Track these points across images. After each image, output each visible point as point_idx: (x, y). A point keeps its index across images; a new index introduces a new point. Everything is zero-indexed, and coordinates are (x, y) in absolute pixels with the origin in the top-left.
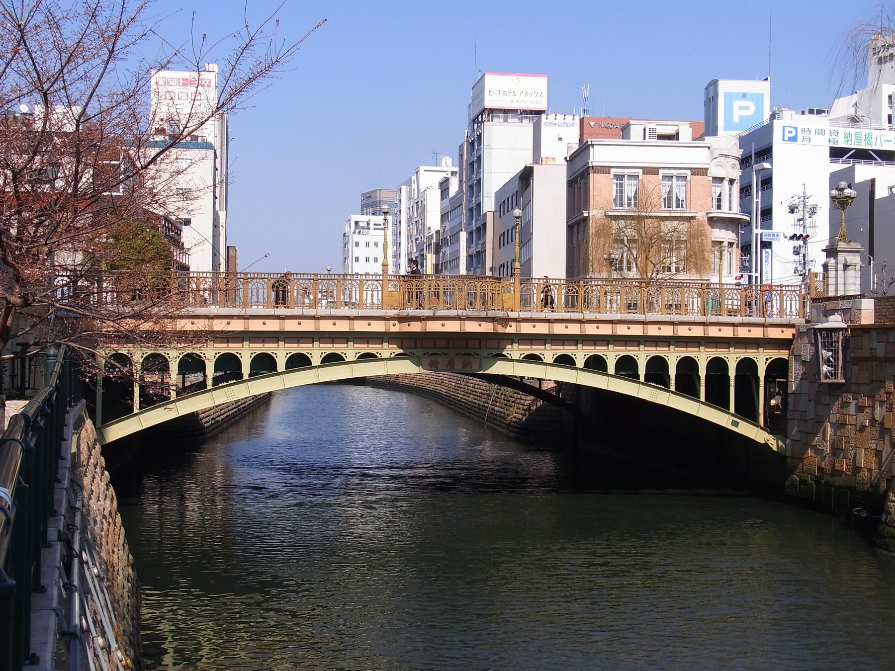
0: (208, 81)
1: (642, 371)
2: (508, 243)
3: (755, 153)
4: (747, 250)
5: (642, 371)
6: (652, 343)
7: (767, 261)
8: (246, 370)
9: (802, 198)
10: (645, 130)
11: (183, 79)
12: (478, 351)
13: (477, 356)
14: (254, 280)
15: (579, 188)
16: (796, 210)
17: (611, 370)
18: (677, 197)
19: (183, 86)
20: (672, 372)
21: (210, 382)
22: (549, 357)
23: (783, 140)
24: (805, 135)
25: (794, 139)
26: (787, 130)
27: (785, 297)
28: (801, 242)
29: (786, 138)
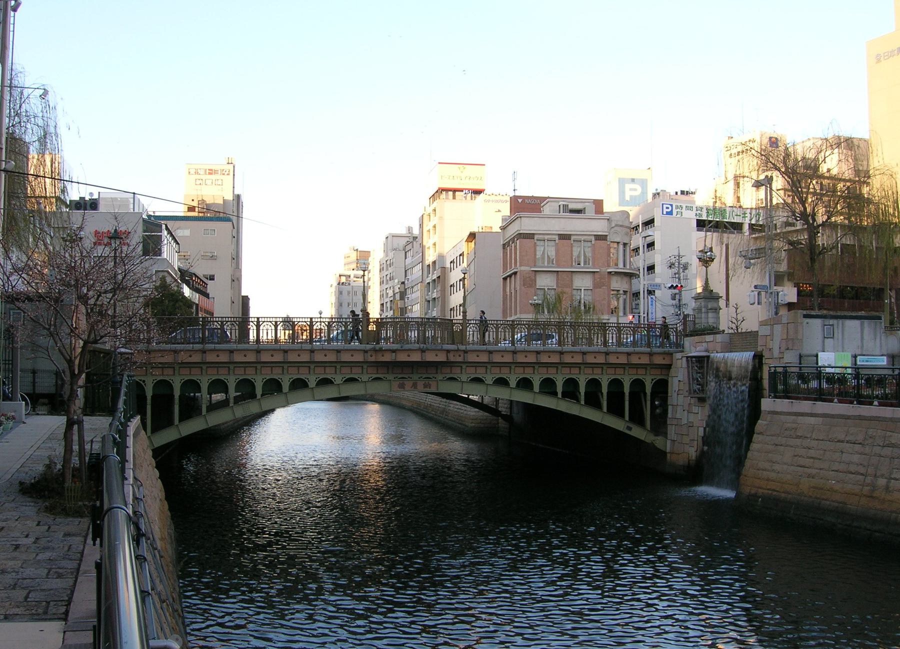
0: (228, 171)
1: (560, 390)
2: (457, 291)
3: (642, 224)
4: (637, 296)
5: (560, 390)
6: (197, 369)
7: (652, 305)
8: (259, 391)
9: (677, 258)
10: (560, 206)
11: (209, 170)
12: (435, 376)
13: (434, 379)
14: (229, 323)
15: (511, 250)
16: (673, 266)
17: (536, 388)
18: (548, 256)
19: (666, 214)
20: (582, 390)
21: (232, 401)
22: (489, 379)
23: (663, 214)
24: (678, 210)
25: (670, 213)
26: (665, 206)
27: (500, 329)
28: (676, 291)
29: (665, 213)
